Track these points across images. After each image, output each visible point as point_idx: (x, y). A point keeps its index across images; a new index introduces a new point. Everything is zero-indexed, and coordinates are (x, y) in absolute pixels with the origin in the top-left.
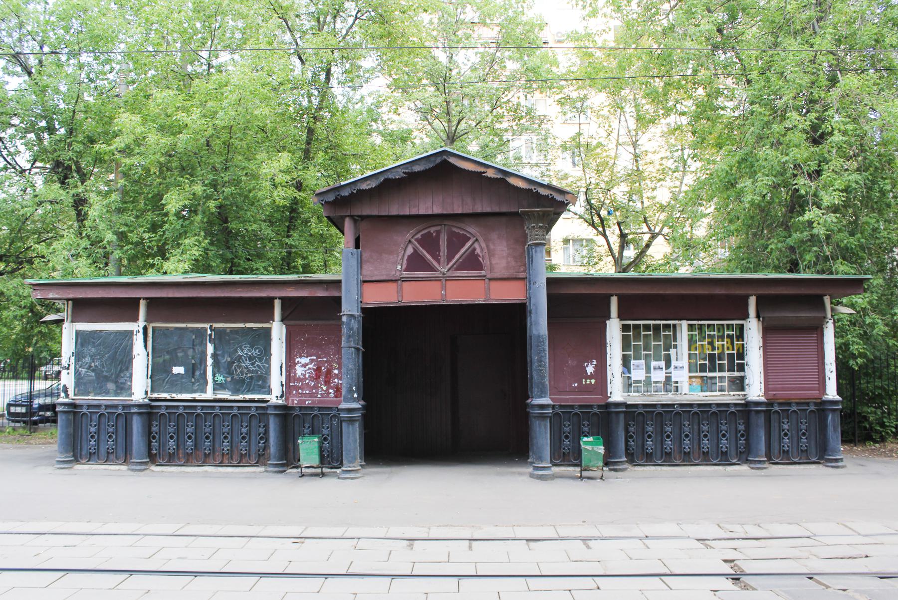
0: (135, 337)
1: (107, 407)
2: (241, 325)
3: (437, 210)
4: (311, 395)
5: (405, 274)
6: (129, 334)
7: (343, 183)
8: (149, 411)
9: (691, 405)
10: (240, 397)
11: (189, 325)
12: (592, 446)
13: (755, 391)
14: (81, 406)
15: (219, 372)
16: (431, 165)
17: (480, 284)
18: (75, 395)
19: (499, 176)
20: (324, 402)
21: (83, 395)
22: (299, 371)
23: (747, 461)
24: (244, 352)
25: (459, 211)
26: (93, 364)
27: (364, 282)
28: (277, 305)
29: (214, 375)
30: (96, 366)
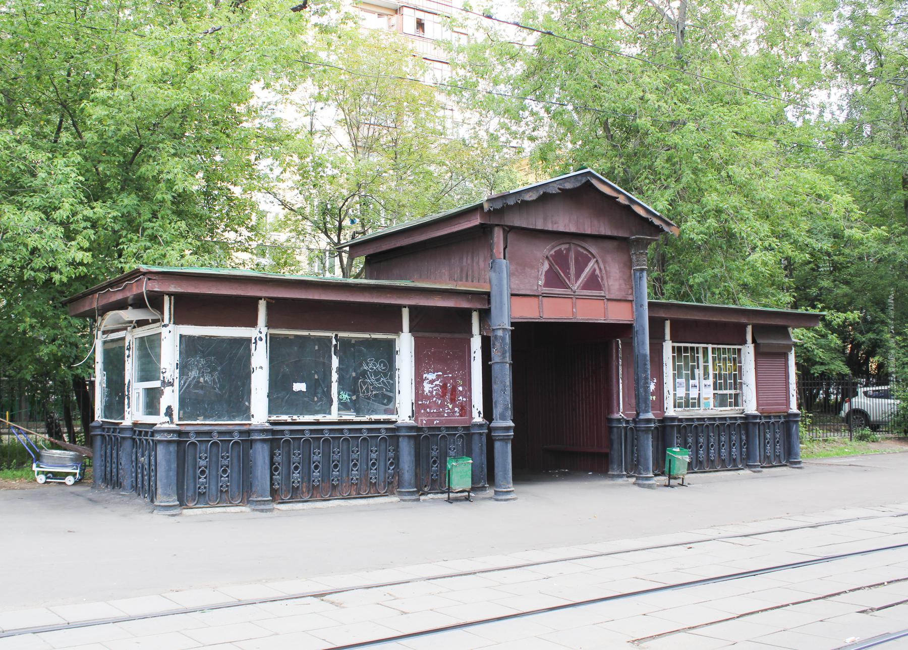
0: (253, 346)
1: (220, 433)
2: (366, 336)
3: (572, 229)
4: (439, 414)
5: (546, 290)
6: (247, 342)
8: (274, 437)
10: (366, 418)
11: (313, 333)
12: (680, 456)
14: (187, 433)
15: (343, 389)
16: (578, 184)
17: (568, 302)
18: (180, 419)
19: (627, 203)
20: (451, 421)
21: (189, 418)
22: (427, 387)
23: (749, 466)
24: (370, 366)
25: (588, 231)
26: (202, 380)
27: (512, 295)
28: (405, 313)
29: (339, 394)
30: (206, 382)
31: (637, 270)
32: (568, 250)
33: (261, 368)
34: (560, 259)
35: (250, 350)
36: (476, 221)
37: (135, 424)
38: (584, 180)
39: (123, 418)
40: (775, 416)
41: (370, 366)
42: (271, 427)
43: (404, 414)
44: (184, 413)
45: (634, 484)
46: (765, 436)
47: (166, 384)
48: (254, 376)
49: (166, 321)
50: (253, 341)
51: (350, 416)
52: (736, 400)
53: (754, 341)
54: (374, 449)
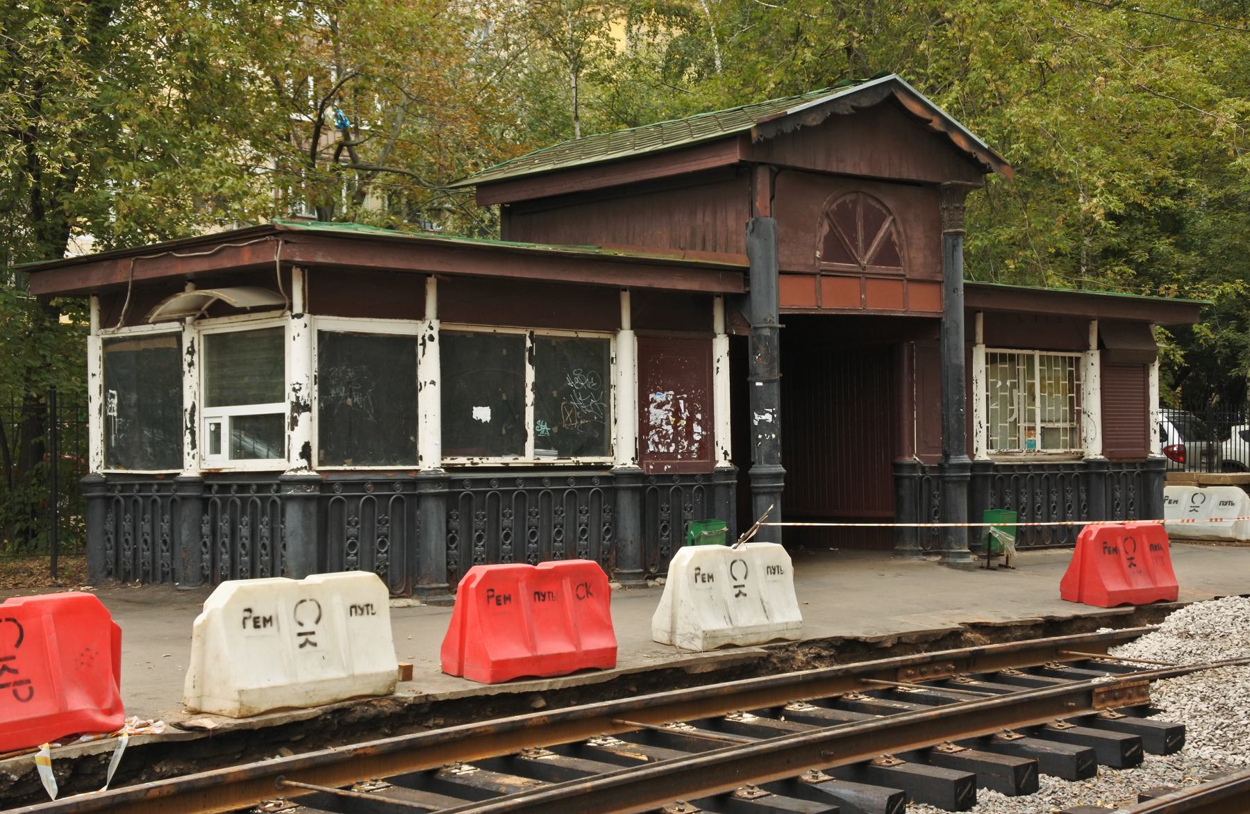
0: (420, 349)
2: (572, 334)
3: (864, 170)
6: (408, 345)
7: (790, 111)
8: (449, 486)
9: (1041, 467)
10: (571, 461)
11: (499, 330)
13: (1094, 449)
16: (878, 100)
17: (854, 284)
18: (321, 463)
19: (941, 129)
24: (575, 381)
26: (349, 401)
27: (781, 273)
30: (355, 404)
31: (949, 234)
32: (854, 203)
33: (433, 383)
34: (842, 219)
35: (416, 355)
36: (733, 156)
37: (209, 475)
38: (886, 95)
39: (181, 467)
40: (1128, 464)
41: (575, 381)
42: (448, 475)
43: (623, 455)
44: (325, 455)
45: (940, 563)
46: (1113, 495)
47: (299, 407)
48: (421, 395)
49: (298, 308)
50: (420, 341)
51: (550, 459)
52: (1075, 432)
53: (1101, 346)
54: (584, 508)
